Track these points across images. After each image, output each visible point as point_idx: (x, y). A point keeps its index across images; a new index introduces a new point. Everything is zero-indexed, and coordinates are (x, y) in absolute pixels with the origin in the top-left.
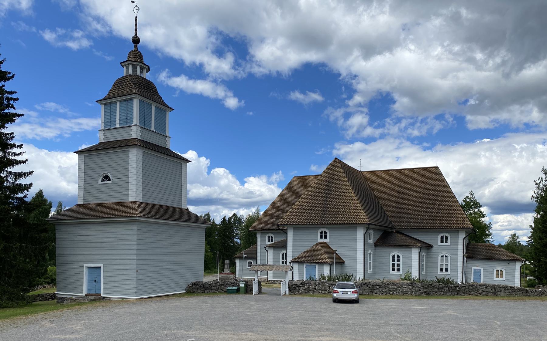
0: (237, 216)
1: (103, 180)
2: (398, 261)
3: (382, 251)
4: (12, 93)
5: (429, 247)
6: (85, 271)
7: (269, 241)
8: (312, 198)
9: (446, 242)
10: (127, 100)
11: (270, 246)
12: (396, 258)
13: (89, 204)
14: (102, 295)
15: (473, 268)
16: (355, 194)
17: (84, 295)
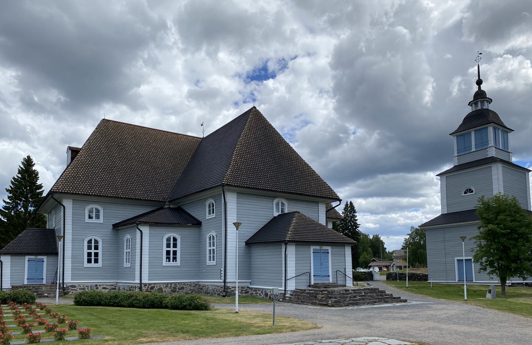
1: (465, 193)
6: (456, 261)
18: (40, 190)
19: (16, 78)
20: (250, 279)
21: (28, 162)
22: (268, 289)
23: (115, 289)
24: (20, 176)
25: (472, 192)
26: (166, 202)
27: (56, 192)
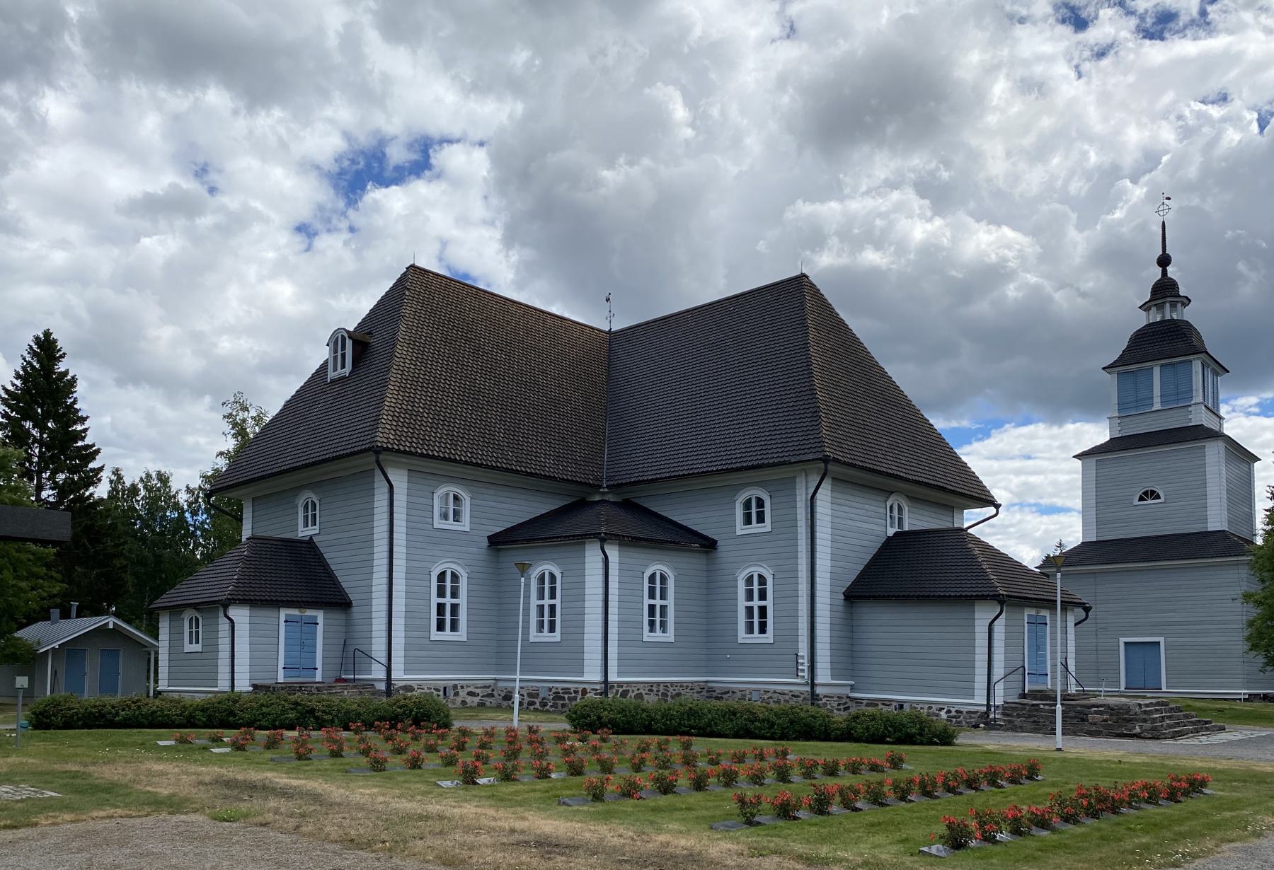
1: (1141, 499)
18: (79, 427)
19: (673, 207)
20: (852, 677)
21: (46, 348)
22: (918, 703)
23: (492, 695)
24: (18, 382)
25: (1158, 497)
26: (600, 487)
27: (387, 449)
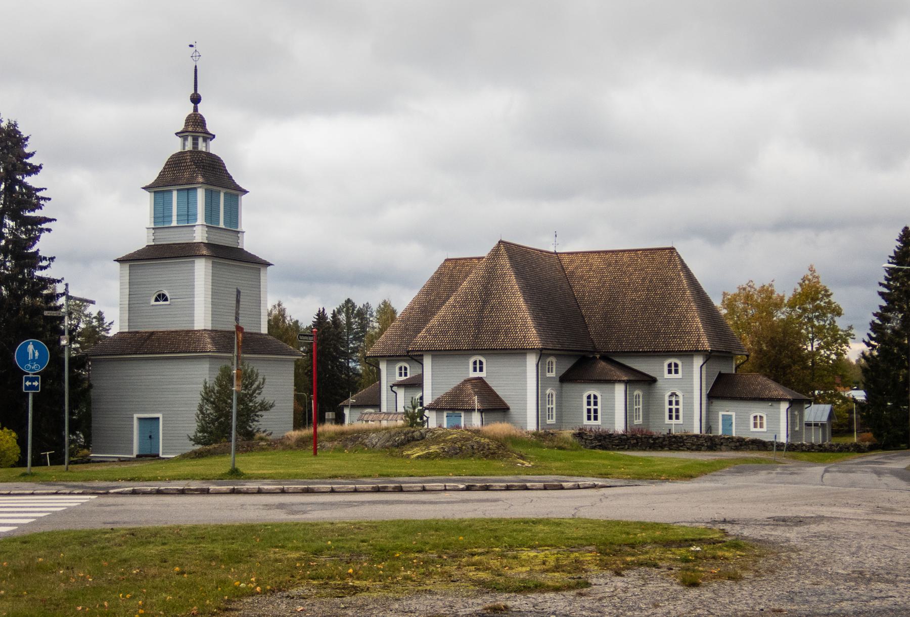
0: (353, 306)
1: (156, 300)
2: (596, 404)
3: (571, 389)
4: (41, 189)
5: (650, 381)
6: (136, 423)
7: (401, 375)
8: (461, 307)
9: (676, 372)
10: (188, 189)
11: (400, 385)
12: (592, 400)
13: (137, 332)
14: (161, 455)
15: (721, 413)
16: (526, 301)
17: (134, 456)
